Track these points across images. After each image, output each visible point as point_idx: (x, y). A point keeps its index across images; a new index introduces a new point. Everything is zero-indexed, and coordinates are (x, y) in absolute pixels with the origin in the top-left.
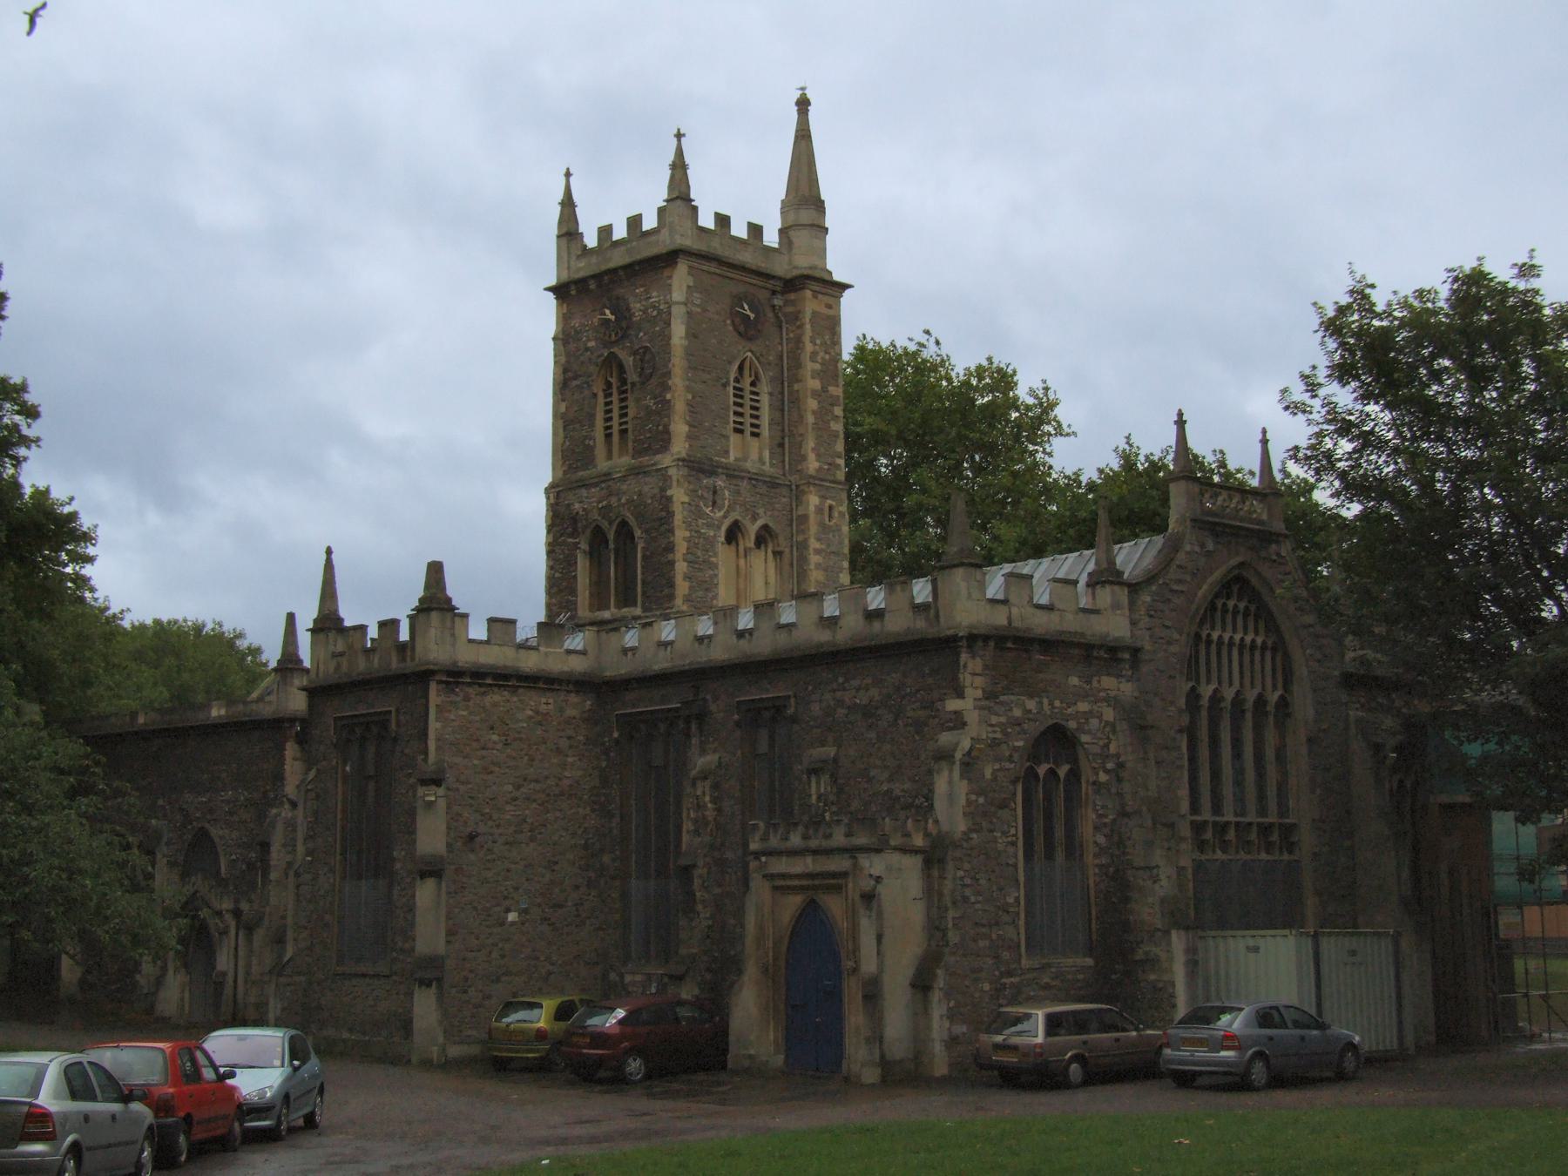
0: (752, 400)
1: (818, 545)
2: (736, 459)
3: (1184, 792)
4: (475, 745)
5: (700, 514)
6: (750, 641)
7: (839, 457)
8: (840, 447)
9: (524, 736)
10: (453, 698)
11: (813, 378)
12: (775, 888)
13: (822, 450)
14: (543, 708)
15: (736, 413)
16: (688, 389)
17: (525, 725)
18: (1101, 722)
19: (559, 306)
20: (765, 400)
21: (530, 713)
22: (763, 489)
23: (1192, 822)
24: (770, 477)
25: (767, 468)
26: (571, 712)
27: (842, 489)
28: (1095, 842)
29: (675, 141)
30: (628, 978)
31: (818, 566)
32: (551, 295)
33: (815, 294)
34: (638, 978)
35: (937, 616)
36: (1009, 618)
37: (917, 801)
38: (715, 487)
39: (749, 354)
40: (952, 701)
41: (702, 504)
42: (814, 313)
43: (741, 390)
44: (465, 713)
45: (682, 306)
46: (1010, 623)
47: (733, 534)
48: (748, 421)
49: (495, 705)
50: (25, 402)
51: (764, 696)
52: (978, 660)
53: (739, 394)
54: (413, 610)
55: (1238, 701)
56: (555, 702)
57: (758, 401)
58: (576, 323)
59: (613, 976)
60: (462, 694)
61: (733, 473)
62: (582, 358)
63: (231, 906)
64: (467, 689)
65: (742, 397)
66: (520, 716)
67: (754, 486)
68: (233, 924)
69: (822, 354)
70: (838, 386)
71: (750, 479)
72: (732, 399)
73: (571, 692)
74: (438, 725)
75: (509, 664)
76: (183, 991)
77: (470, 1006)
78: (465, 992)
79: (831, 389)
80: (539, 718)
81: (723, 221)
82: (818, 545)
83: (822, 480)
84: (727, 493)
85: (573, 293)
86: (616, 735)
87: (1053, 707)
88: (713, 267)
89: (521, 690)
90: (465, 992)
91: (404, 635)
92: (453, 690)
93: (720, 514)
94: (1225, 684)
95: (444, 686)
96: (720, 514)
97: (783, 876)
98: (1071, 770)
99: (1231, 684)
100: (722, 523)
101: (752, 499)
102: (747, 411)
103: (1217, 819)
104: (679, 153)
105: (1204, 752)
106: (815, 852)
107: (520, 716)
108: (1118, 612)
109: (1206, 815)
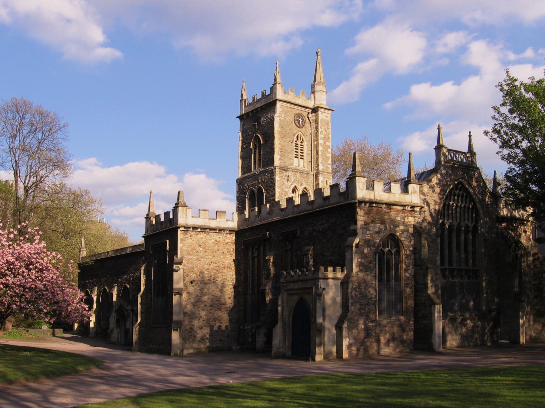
0: (301, 147)
2: (296, 166)
3: (438, 258)
4: (194, 251)
5: (284, 184)
6: (285, 212)
7: (330, 165)
8: (330, 161)
9: (211, 248)
10: (186, 236)
11: (321, 139)
12: (288, 294)
13: (324, 163)
14: (218, 239)
15: (296, 152)
16: (280, 144)
17: (212, 245)
18: (408, 233)
19: (241, 122)
20: (305, 148)
21: (214, 241)
22: (304, 175)
23: (441, 269)
24: (307, 172)
25: (306, 169)
26: (228, 240)
27: (330, 175)
28: (405, 276)
30: (246, 327)
32: (238, 119)
34: (249, 327)
35: (348, 196)
36: (374, 196)
37: (340, 263)
38: (288, 175)
39: (300, 133)
40: (353, 226)
41: (284, 181)
42: (321, 119)
43: (297, 144)
44: (190, 241)
45: (278, 117)
46: (375, 198)
48: (300, 154)
49: (201, 238)
51: (289, 230)
52: (362, 211)
53: (297, 145)
54: (173, 207)
55: (459, 226)
56: (222, 237)
57: (303, 148)
58: (245, 127)
59: (242, 327)
60: (189, 235)
61: (295, 171)
62: (247, 138)
63: (131, 308)
64: (191, 233)
65: (298, 147)
66: (210, 242)
67: (301, 174)
68: (132, 313)
69: (324, 132)
70: (329, 142)
71: (300, 172)
72: (294, 147)
73: (228, 233)
74: (181, 245)
75: (206, 224)
76: (118, 335)
77: (192, 337)
78: (191, 332)
79: (327, 143)
80: (217, 242)
83: (324, 172)
84: (292, 177)
85: (245, 118)
86: (242, 248)
87: (390, 228)
88: (288, 105)
89: (210, 233)
90: (191, 332)
91: (171, 216)
92: (186, 233)
93: (290, 184)
94: (455, 221)
95: (183, 232)
96: (290, 184)
97: (292, 290)
98: (397, 251)
99: (456, 221)
100: (291, 187)
101: (301, 179)
102: (299, 151)
103: (451, 268)
106: (302, 281)
107: (210, 242)
108: (415, 194)
109: (446, 266)
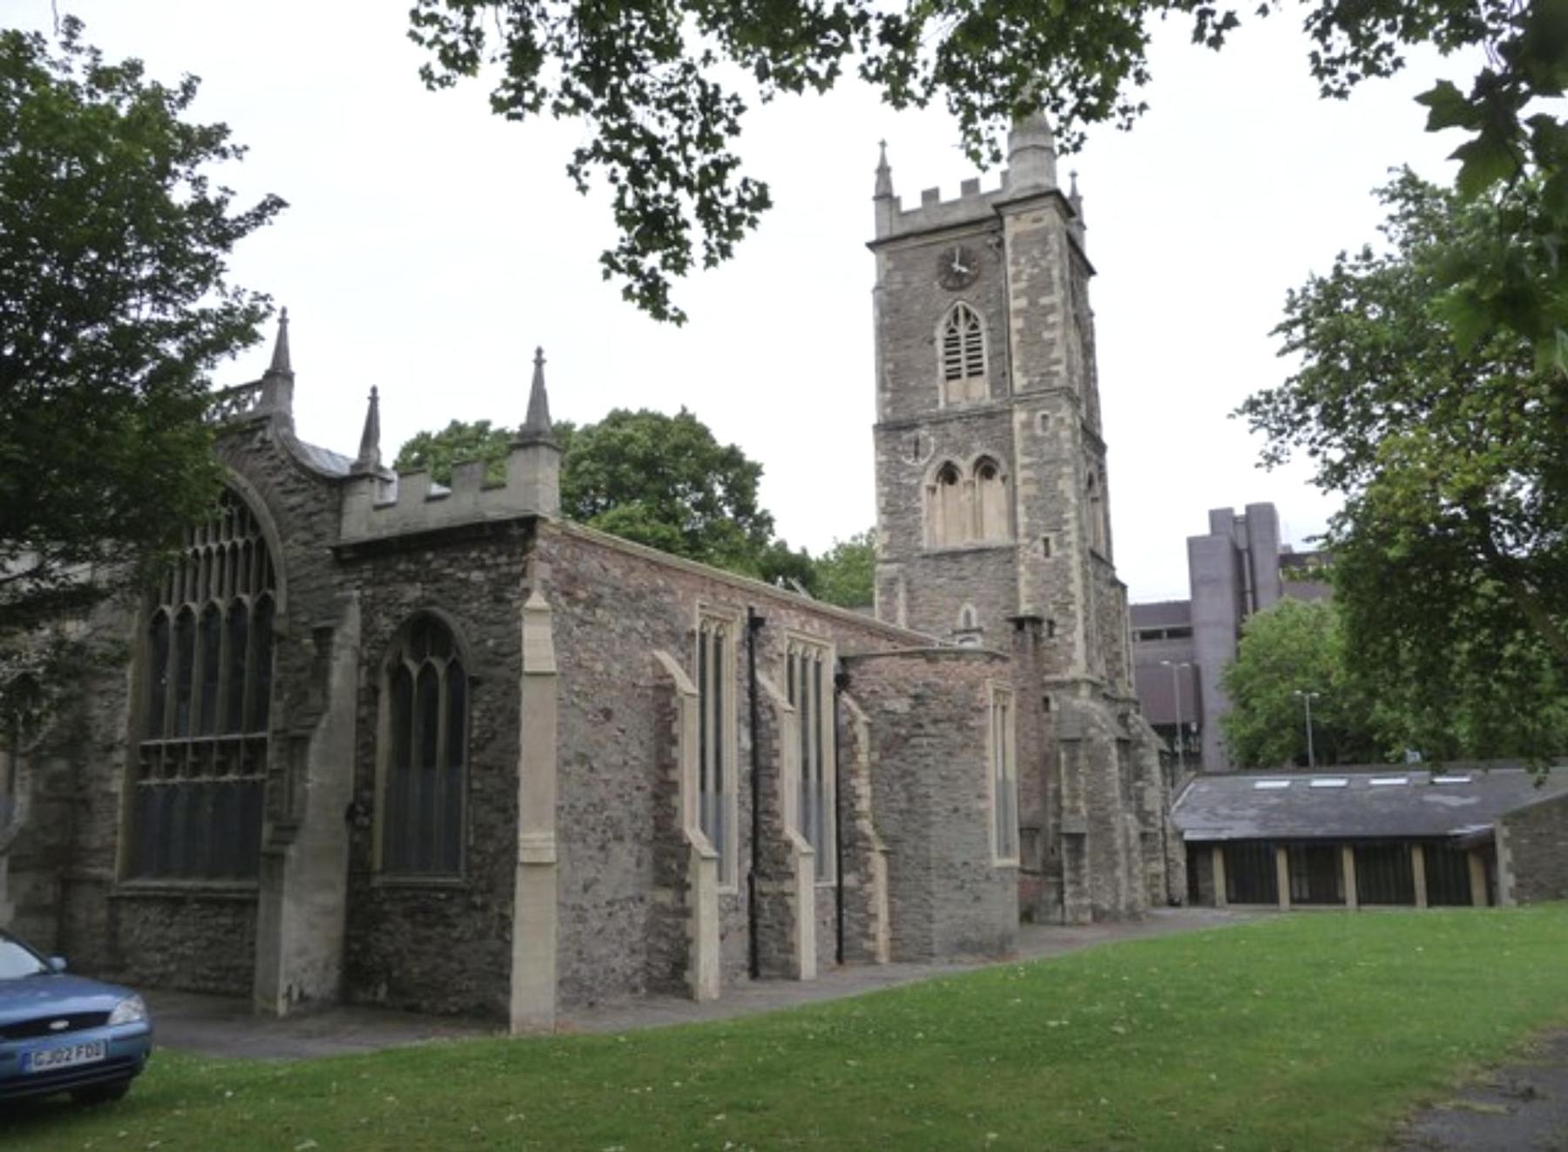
1: (1027, 460)
29: (878, 149)
31: (1026, 481)
33: (1017, 217)
47: (949, 474)
50: (565, 430)
54: (1261, 393)
81: (930, 195)
82: (1027, 460)
88: (912, 242)
96: (923, 462)
104: (883, 158)
105: (417, 726)
